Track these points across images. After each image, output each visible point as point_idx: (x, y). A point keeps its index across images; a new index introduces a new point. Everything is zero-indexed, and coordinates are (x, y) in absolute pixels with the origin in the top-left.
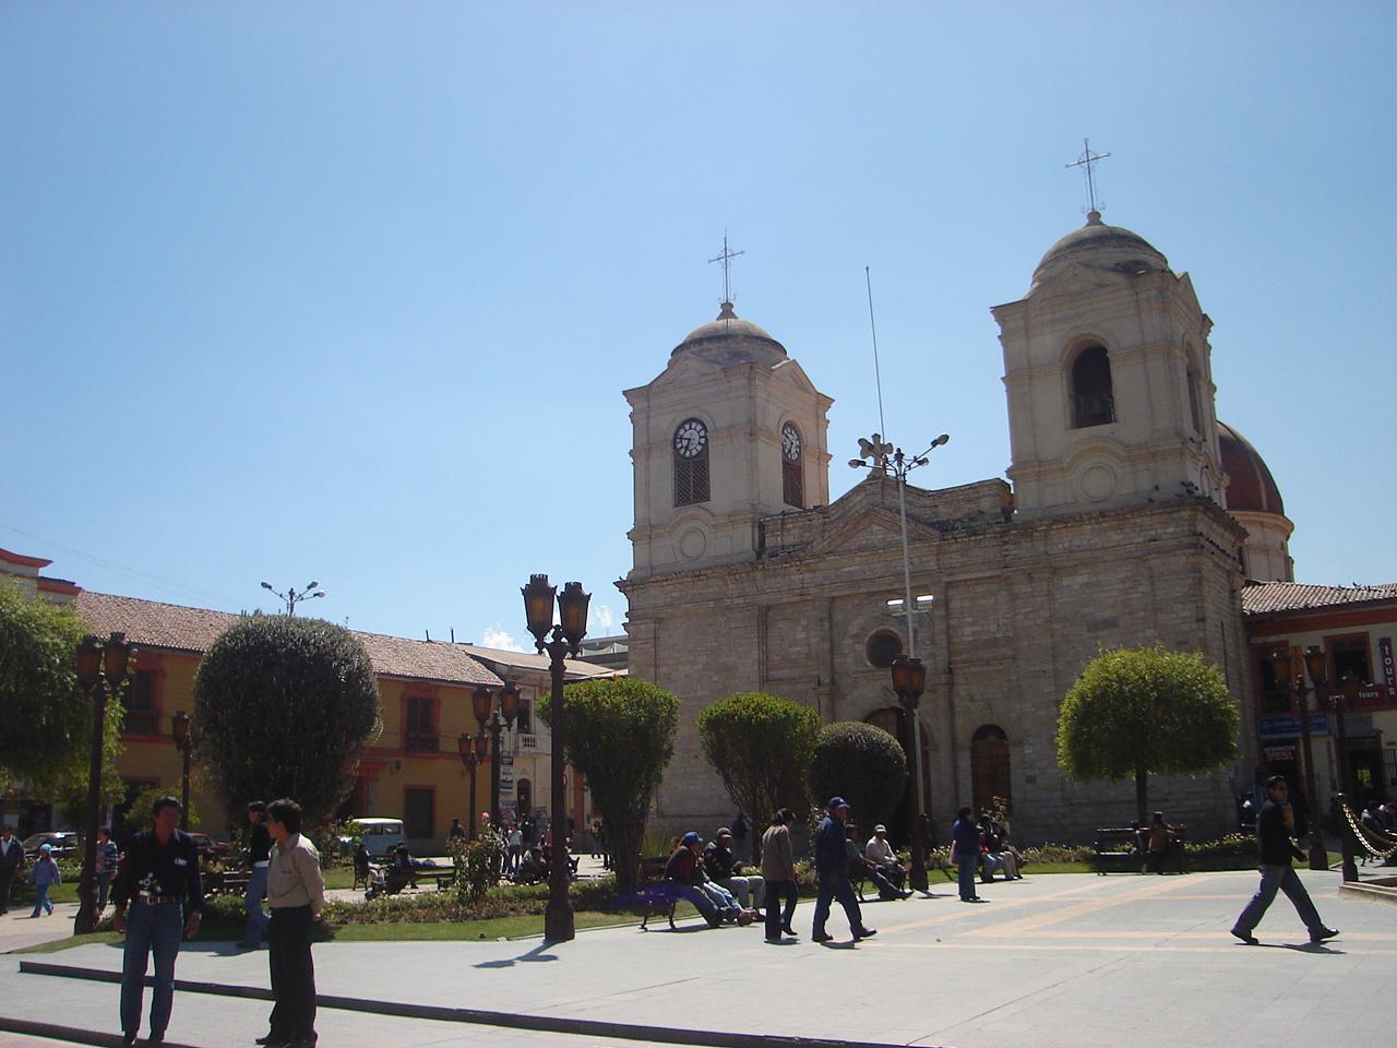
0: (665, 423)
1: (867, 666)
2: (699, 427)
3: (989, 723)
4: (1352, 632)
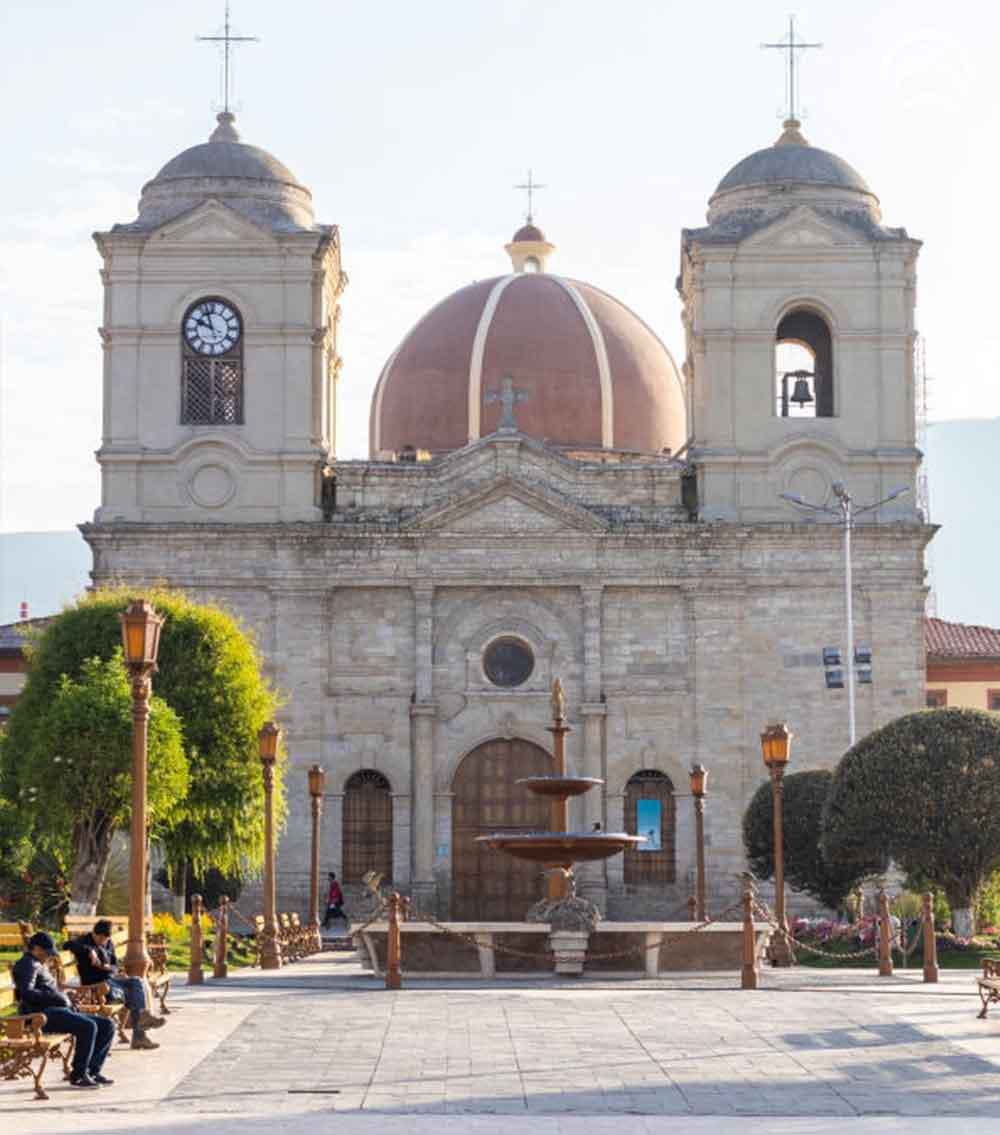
0: (164, 306)
1: (481, 682)
2: (228, 313)
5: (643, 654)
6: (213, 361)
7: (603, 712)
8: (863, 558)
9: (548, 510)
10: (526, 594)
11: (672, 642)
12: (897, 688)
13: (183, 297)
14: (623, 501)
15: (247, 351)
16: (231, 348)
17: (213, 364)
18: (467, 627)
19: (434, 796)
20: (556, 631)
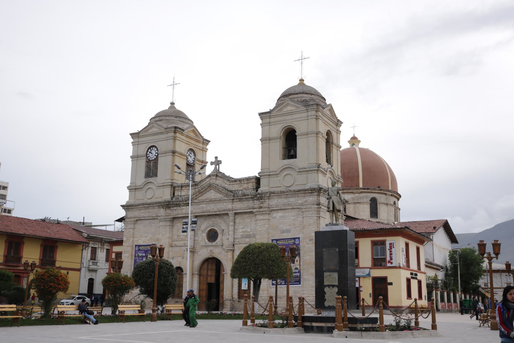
2: (156, 149)
3: (179, 266)
4: (382, 238)
5: (245, 232)
6: (152, 161)
7: (233, 249)
8: (301, 199)
9: (220, 192)
10: (218, 217)
11: (252, 228)
12: (311, 239)
13: (147, 147)
14: (241, 188)
15: (159, 158)
16: (156, 158)
17: (152, 162)
18: (203, 227)
19: (193, 274)
20: (224, 226)
